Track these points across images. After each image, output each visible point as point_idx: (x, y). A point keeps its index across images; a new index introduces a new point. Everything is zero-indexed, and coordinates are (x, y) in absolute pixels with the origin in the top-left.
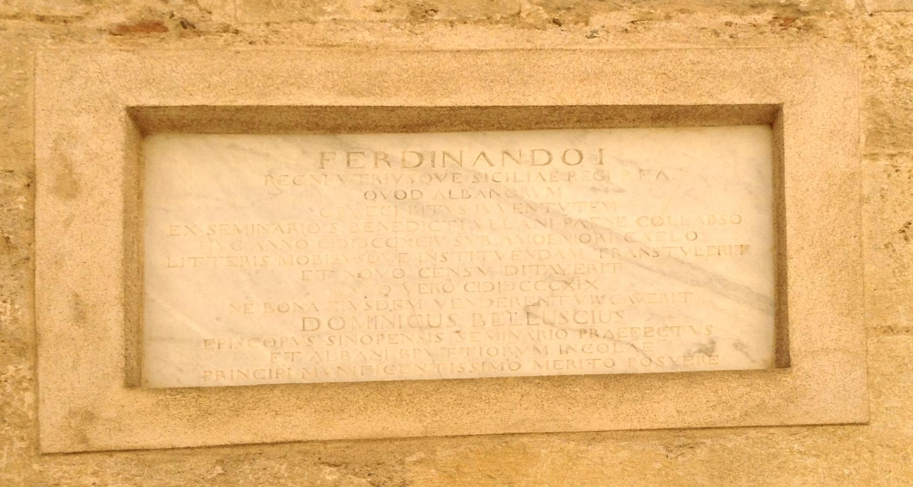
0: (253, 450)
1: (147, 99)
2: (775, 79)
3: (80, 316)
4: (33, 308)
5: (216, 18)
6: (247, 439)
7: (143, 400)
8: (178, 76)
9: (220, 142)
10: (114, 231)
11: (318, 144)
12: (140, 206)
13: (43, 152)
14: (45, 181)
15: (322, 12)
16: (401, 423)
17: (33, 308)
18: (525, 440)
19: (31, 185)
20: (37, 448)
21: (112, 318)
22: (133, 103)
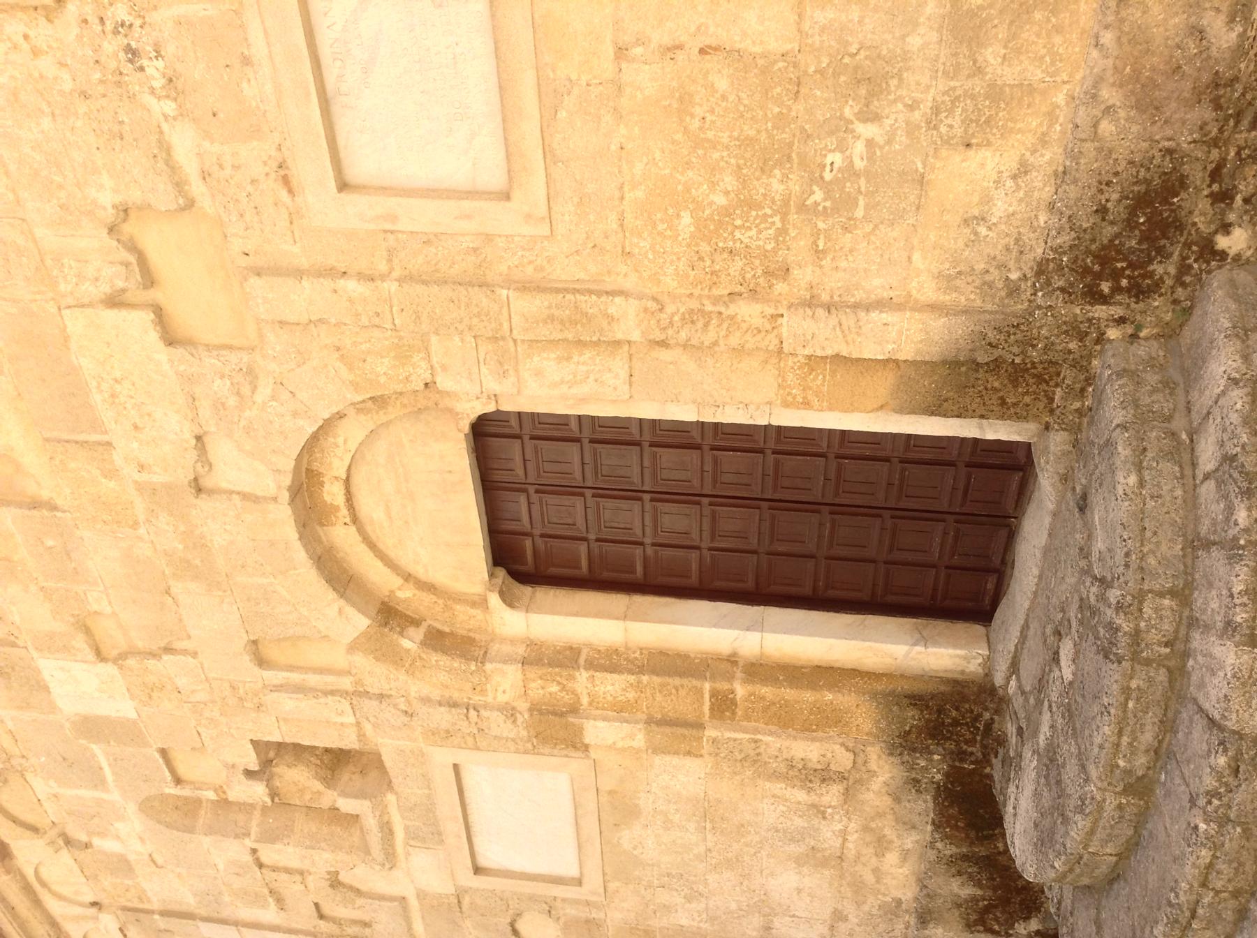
0: (547, 149)
1: (332, 184)
2: (1075, 181)
3: (469, 217)
4: (463, 235)
5: (273, 153)
6: (540, 151)
7: (516, 195)
8: (312, 169)
9: (342, 155)
10: (414, 202)
11: (336, 109)
12: (391, 188)
13: (372, 226)
14: (388, 226)
15: (258, 107)
16: (527, 81)
17: (463, 235)
18: (536, 16)
19: (392, 232)
20: (546, 237)
21: (466, 205)
22: (1040, 461)
